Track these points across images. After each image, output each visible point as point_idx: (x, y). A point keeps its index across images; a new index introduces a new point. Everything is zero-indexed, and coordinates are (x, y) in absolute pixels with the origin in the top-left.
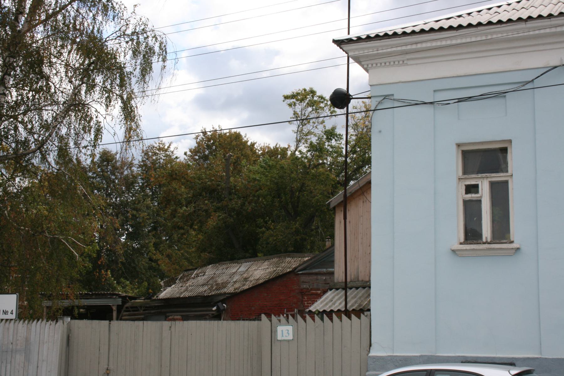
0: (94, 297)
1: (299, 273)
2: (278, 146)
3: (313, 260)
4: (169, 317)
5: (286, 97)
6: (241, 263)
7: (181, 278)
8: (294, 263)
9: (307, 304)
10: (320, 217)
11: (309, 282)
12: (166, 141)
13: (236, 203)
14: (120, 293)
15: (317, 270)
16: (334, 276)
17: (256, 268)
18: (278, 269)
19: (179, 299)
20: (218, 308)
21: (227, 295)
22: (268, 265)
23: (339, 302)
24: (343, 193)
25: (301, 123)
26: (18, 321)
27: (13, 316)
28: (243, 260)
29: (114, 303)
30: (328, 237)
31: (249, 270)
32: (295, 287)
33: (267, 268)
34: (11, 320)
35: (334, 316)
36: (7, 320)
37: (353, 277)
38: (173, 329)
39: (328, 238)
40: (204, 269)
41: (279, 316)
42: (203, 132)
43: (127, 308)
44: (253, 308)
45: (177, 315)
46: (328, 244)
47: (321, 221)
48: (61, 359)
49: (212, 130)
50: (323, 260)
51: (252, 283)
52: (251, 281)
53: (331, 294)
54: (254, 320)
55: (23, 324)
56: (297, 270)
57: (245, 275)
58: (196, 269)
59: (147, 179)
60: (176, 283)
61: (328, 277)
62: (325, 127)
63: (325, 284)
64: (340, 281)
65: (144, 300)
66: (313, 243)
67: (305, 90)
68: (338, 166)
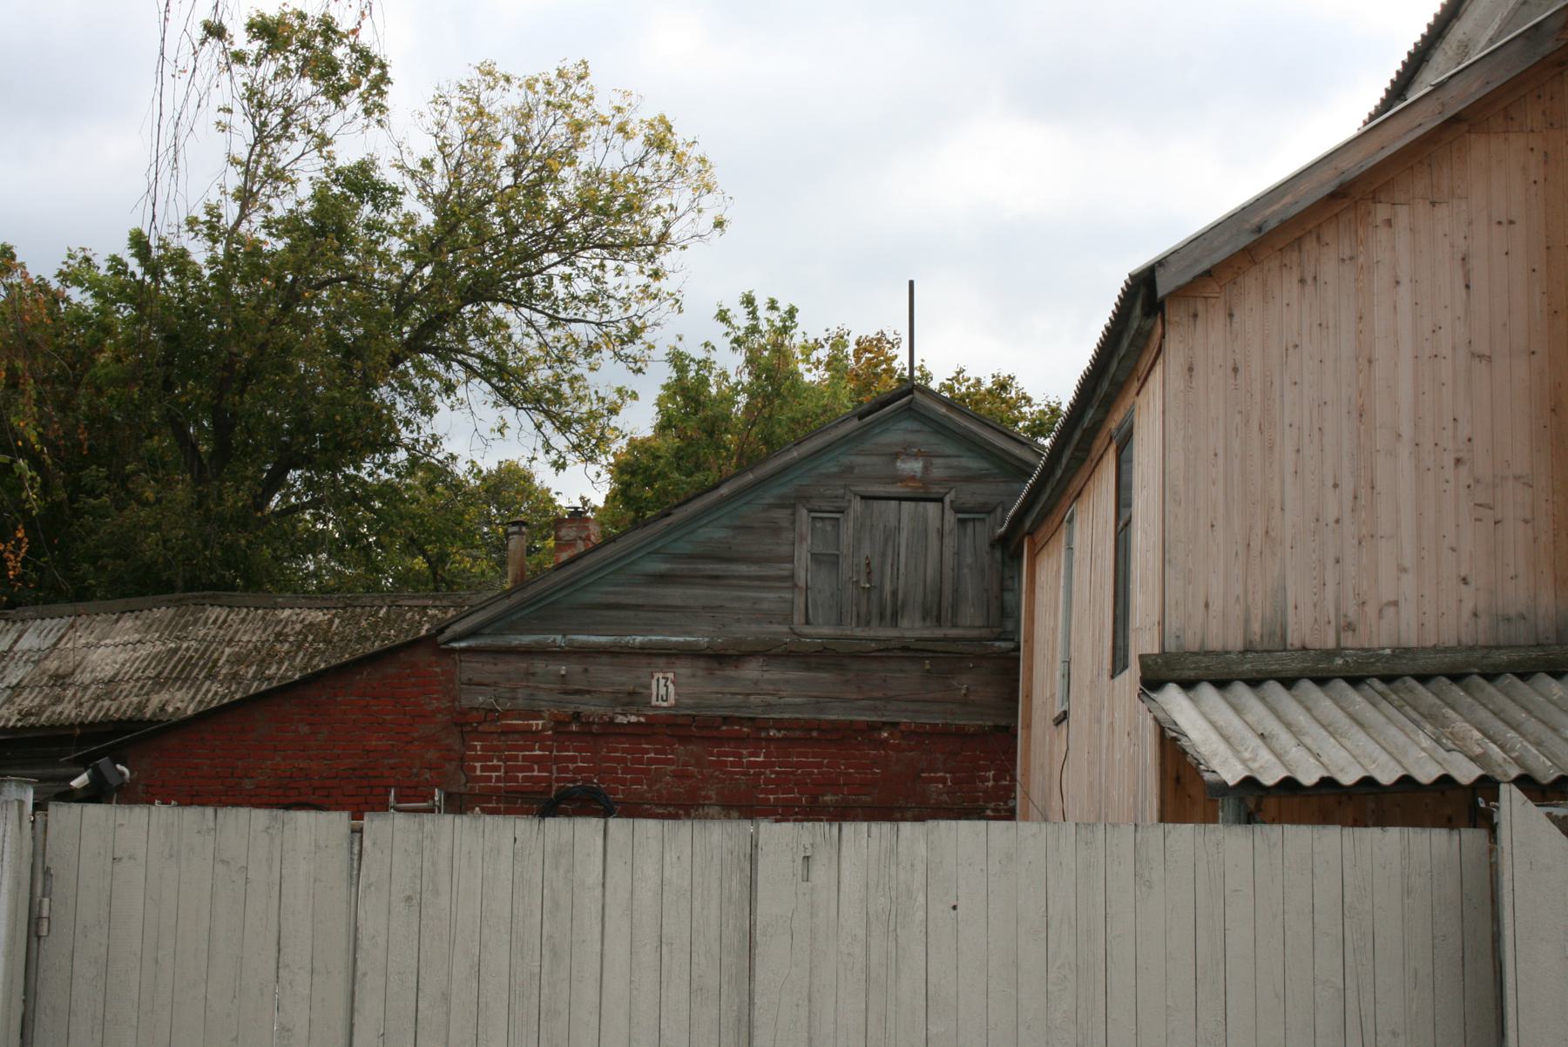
1: (455, 645)
8: (243, 628)
9: (484, 769)
11: (495, 684)
15: (527, 639)
17: (92, 639)
18: (185, 645)
32: (435, 704)
33: (139, 641)
37: (1256, 627)
38: (820, 872)
51: (89, 692)
56: (448, 633)
57: (52, 665)
62: (330, 157)
63: (566, 693)
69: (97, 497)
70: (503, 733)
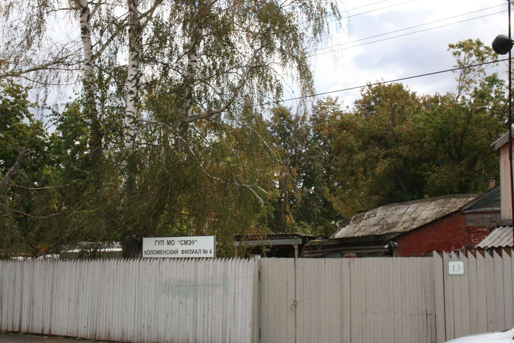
0: (277, 238)
1: (465, 212)
2: (437, 95)
3: (478, 200)
4: (344, 254)
5: (452, 46)
6: (409, 204)
7: (354, 219)
8: (459, 203)
10: (483, 159)
11: (475, 220)
12: (333, 96)
13: (404, 150)
14: (300, 234)
15: (482, 209)
16: (500, 215)
17: (424, 209)
18: (444, 209)
19: (353, 238)
20: (390, 246)
21: (397, 234)
22: (434, 206)
23: (507, 238)
24: (509, 135)
25: (464, 72)
26: (216, 259)
27: (212, 255)
28: (411, 202)
29: (295, 242)
30: (492, 178)
31: (416, 210)
32: (462, 226)
33: (434, 209)
34: (211, 258)
35: (503, 252)
36: (207, 258)
38: (352, 265)
39: (492, 179)
40: (375, 210)
41: (450, 252)
42: (368, 85)
43: (307, 247)
44: (423, 246)
45: (352, 253)
46: (492, 184)
47: (484, 163)
48: (254, 292)
49: (376, 82)
50: (489, 199)
52: (419, 221)
53: (498, 232)
54: (424, 256)
55: (221, 261)
56: (463, 209)
57: (413, 216)
58: (367, 210)
59: (317, 130)
60: (349, 224)
61: (493, 216)
63: (491, 222)
64: (507, 218)
65: (322, 239)
66: (477, 184)
67: (471, 41)
68: (499, 110)
69: (426, 172)
70: (478, 232)
